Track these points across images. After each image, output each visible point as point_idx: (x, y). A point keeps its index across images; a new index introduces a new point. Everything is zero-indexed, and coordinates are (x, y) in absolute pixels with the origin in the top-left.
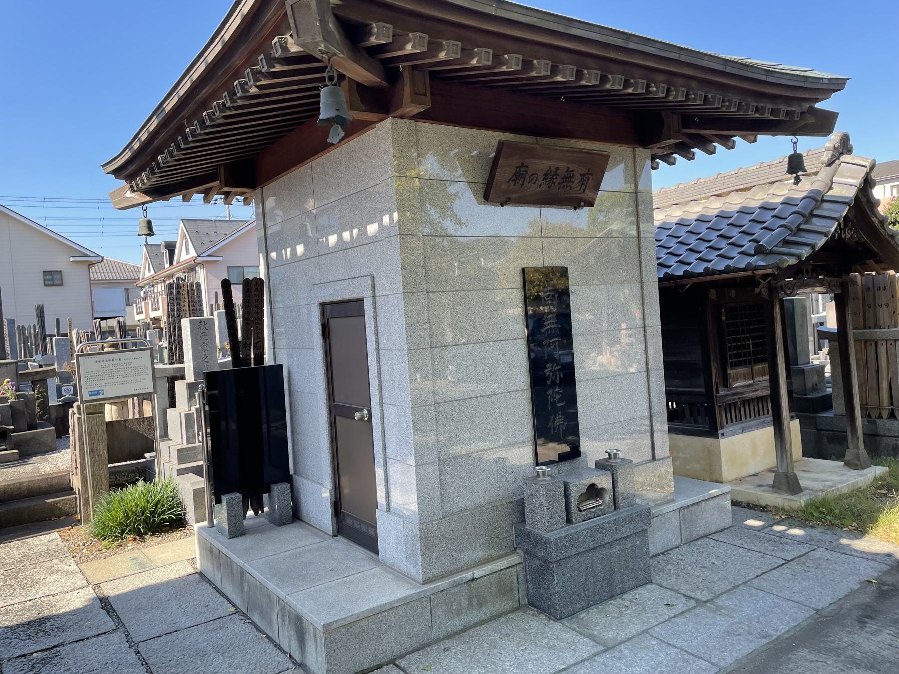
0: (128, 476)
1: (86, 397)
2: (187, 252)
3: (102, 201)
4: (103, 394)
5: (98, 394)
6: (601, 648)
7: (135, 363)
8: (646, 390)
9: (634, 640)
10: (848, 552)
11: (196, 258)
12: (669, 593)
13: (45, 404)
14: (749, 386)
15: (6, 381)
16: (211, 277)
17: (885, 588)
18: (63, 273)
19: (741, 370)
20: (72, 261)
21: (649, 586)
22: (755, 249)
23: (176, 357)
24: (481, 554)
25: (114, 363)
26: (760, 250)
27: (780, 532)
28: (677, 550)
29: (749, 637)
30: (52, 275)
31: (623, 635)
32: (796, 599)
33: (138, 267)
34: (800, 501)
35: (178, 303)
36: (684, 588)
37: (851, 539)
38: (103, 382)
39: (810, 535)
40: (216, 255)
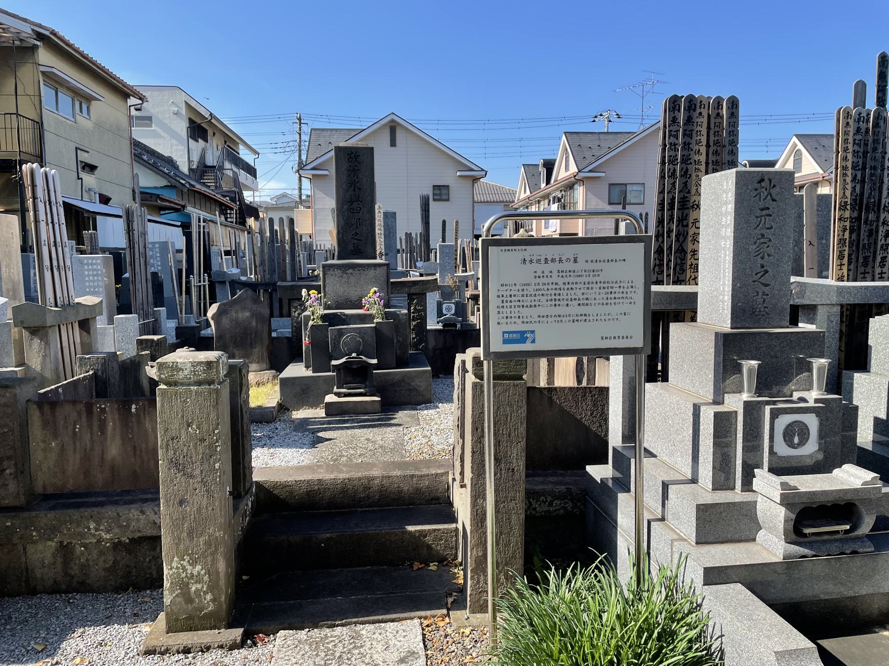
0: (551, 504)
1: (497, 345)
2: (567, 168)
3: (487, 122)
4: (533, 341)
5: (523, 340)
7: (610, 273)
11: (577, 173)
13: (421, 327)
15: (372, 290)
16: (590, 195)
18: (450, 189)
20: (459, 176)
23: (668, 268)
25: (562, 267)
30: (440, 190)
33: (513, 191)
35: (687, 146)
38: (535, 312)
40: (598, 171)
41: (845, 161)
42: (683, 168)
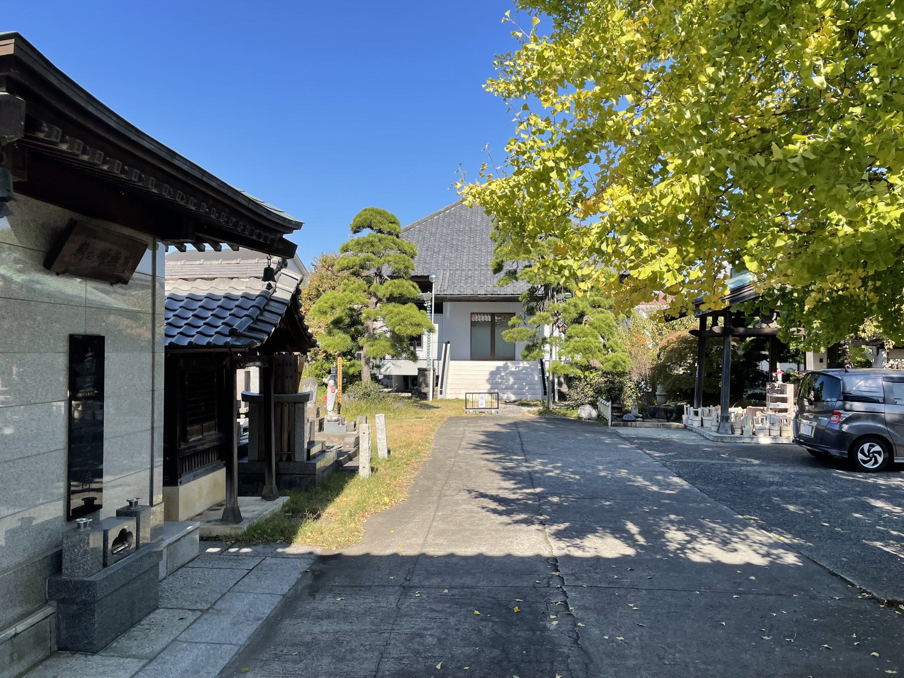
6: (145, 661)
8: (150, 448)
9: (168, 648)
10: (288, 557)
12: (177, 611)
14: (200, 440)
17: (316, 573)
19: (197, 427)
21: (157, 611)
22: (230, 332)
24: (19, 610)
26: (233, 333)
27: (235, 552)
28: (165, 581)
29: (249, 622)
31: (157, 648)
32: (267, 591)
34: (244, 527)
36: (186, 605)
37: (284, 548)
39: (256, 551)
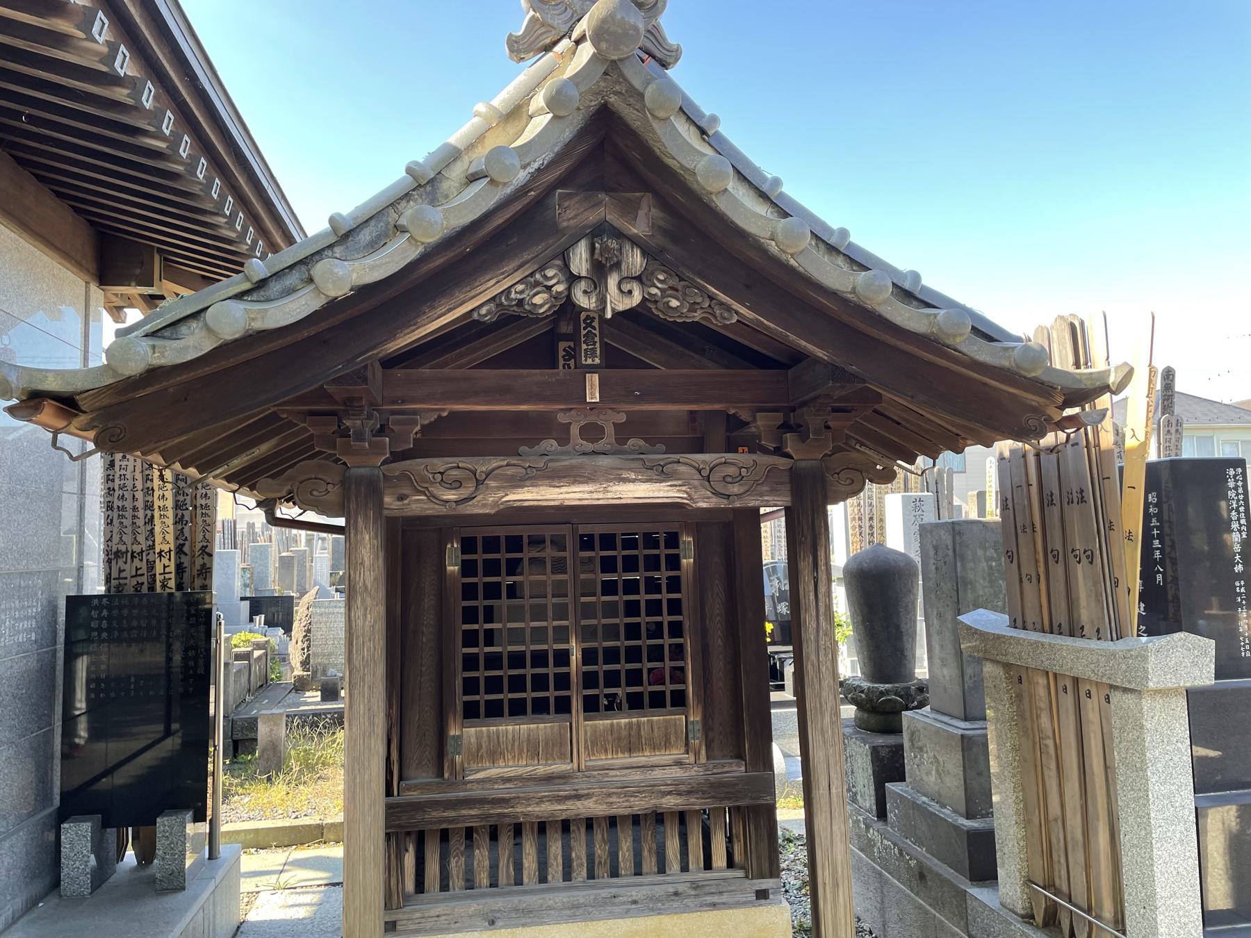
41: (121, 501)
42: (177, 515)
